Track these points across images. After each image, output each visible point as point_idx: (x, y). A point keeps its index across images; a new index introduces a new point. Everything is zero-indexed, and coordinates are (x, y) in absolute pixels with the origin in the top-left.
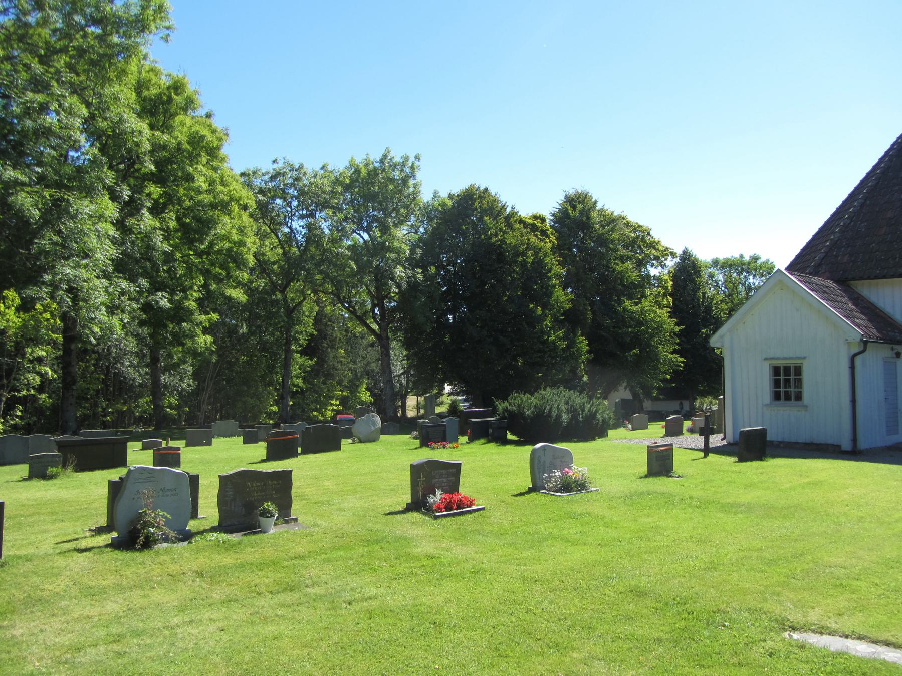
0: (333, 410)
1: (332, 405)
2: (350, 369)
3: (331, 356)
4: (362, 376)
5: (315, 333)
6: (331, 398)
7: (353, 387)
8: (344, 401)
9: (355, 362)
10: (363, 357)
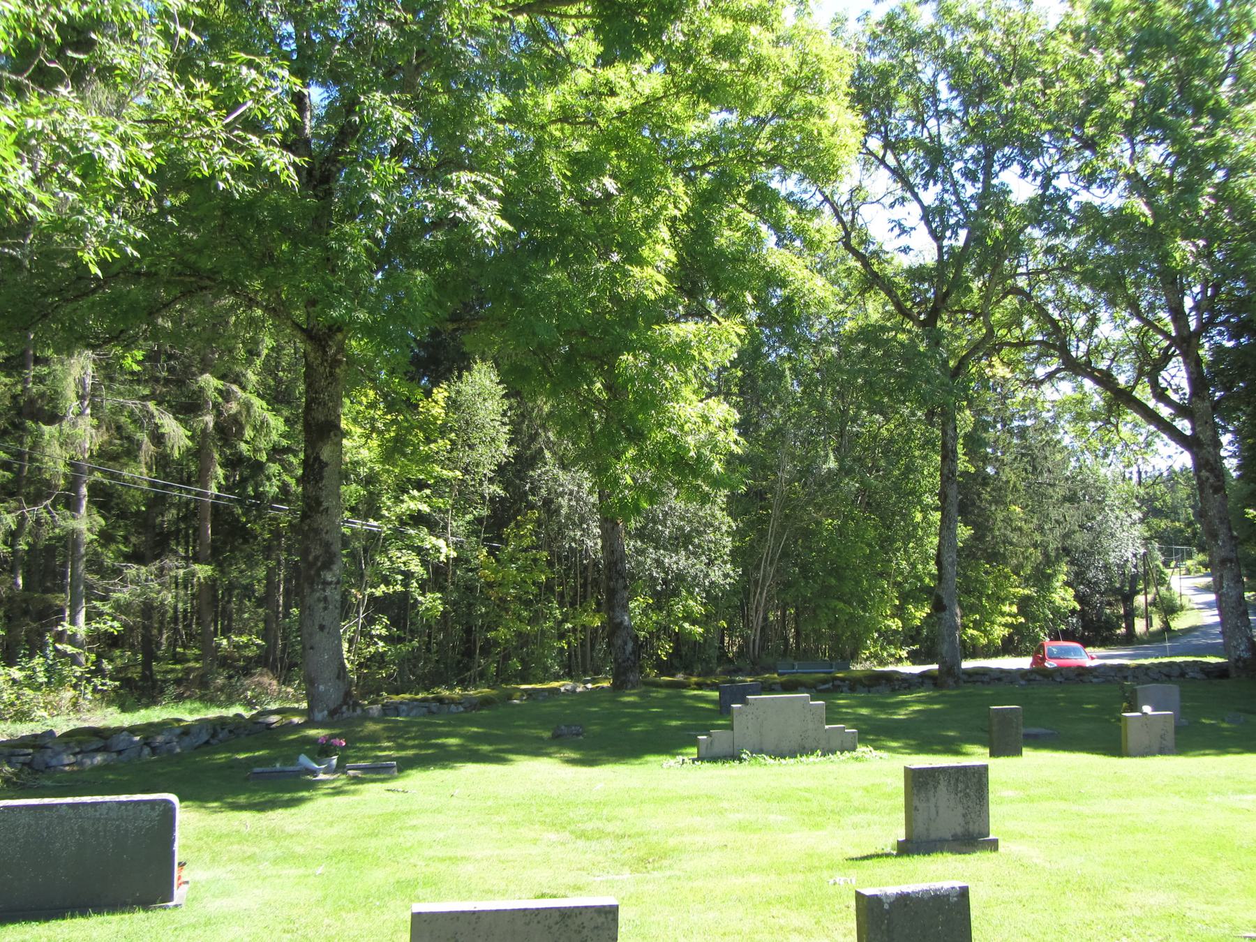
0: (1006, 625)
1: (1003, 614)
2: (1035, 546)
3: (1000, 516)
4: (1058, 559)
5: (972, 470)
6: (1002, 600)
7: (1042, 579)
8: (1024, 604)
9: (1040, 529)
10: (1057, 521)
